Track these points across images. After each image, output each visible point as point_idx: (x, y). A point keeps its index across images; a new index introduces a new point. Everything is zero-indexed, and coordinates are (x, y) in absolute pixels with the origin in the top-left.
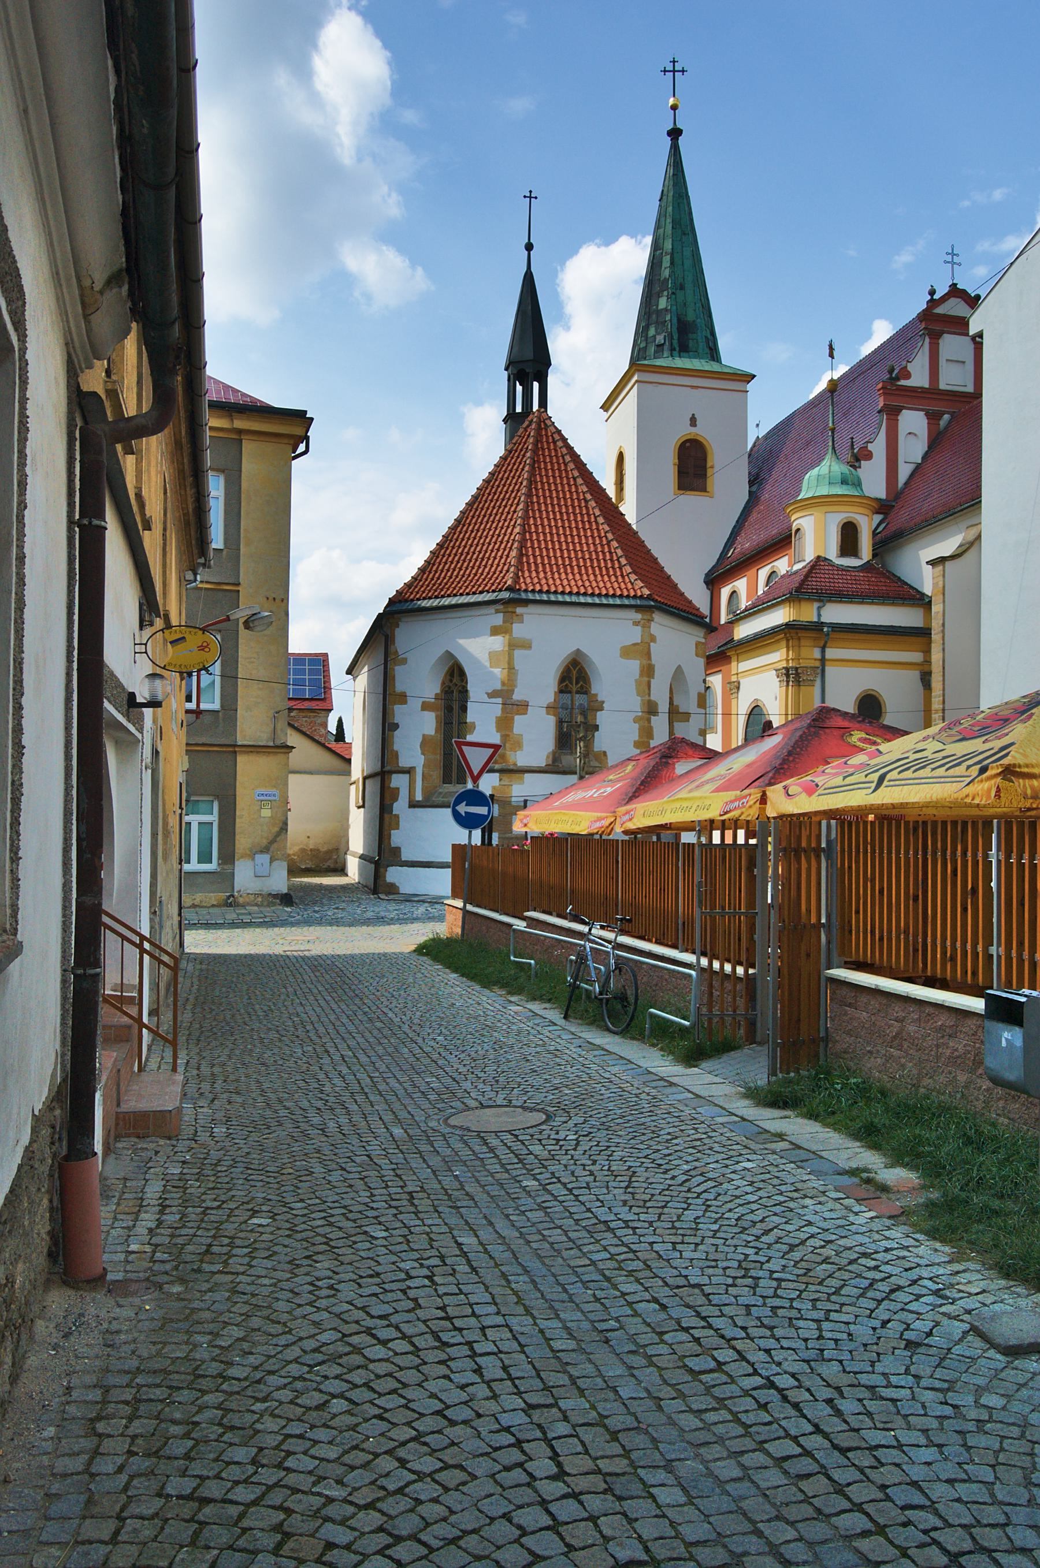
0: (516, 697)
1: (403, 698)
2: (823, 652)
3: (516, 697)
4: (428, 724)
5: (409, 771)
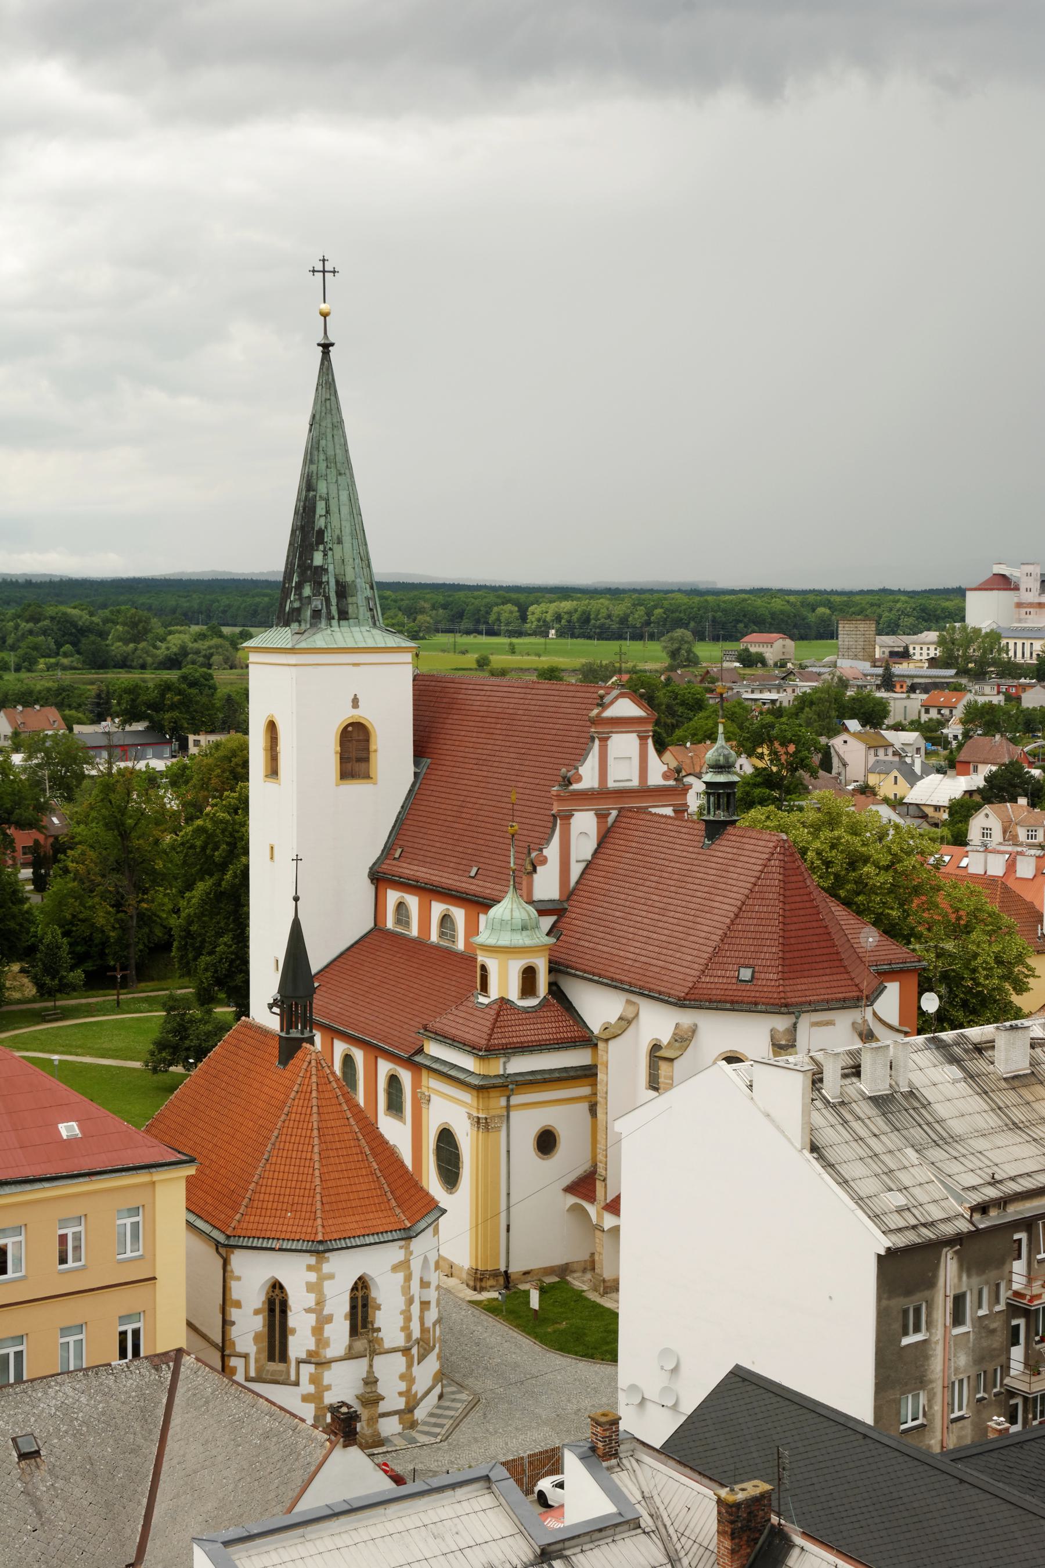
0: (326, 1312)
1: (238, 1304)
2: (508, 1101)
3: (326, 1312)
4: (258, 1323)
5: (246, 1356)
